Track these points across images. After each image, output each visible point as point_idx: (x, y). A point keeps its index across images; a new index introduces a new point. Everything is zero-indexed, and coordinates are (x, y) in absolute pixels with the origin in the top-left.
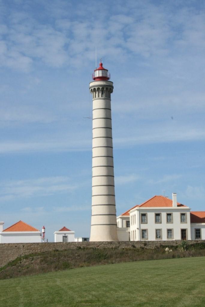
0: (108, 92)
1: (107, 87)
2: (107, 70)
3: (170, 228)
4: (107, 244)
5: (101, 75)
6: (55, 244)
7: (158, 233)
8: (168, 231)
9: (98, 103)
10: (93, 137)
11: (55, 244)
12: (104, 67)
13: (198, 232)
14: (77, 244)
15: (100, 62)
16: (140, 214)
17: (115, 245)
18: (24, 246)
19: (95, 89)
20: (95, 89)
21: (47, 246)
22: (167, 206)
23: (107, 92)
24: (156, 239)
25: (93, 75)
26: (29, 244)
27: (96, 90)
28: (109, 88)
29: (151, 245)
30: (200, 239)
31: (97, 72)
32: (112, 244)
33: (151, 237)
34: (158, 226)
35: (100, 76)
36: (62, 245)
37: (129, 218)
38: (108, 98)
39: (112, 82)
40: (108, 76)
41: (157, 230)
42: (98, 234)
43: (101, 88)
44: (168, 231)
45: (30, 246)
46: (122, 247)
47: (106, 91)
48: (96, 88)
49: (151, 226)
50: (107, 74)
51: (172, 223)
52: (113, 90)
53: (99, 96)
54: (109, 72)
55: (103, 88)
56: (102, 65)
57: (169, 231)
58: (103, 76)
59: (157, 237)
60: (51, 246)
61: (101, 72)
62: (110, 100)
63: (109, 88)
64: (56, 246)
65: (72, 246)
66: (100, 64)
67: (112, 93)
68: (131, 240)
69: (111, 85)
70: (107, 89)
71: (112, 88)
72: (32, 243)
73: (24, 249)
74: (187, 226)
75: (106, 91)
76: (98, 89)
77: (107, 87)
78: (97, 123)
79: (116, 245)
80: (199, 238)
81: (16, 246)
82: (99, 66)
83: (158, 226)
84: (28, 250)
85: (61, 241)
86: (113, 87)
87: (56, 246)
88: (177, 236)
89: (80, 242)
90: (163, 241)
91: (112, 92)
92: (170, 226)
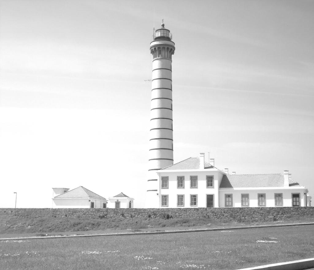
0: (169, 52)
5: (159, 35)
6: (42, 210)
7: (181, 199)
11: (42, 210)
14: (50, 210)
16: (161, 178)
17: (103, 213)
18: (12, 212)
19: (168, 48)
21: (34, 212)
22: (194, 168)
23: (168, 51)
26: (17, 210)
28: (170, 48)
29: (143, 214)
30: (184, 206)
32: (99, 212)
33: (173, 204)
34: (181, 192)
36: (48, 211)
37: (209, 186)
39: (174, 43)
41: (179, 196)
45: (18, 211)
46: (22, 211)
49: (173, 191)
50: (169, 35)
51: (197, 188)
55: (159, 48)
56: (163, 25)
57: (194, 199)
59: (178, 204)
63: (170, 48)
64: (42, 212)
65: (58, 213)
69: (173, 45)
71: (173, 49)
72: (19, 209)
73: (12, 215)
74: (215, 191)
81: (5, 212)
83: (181, 192)
84: (16, 216)
86: (174, 48)
87: (42, 212)
88: (202, 203)
89: (124, 209)
91: (173, 53)
92: (194, 192)
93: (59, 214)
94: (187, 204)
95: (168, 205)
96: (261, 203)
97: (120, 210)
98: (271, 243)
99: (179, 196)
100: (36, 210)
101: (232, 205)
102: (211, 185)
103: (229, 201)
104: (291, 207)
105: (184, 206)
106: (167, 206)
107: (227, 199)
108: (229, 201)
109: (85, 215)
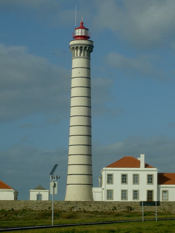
1: (90, 47)
2: (88, 29)
3: (136, 189)
4: (64, 203)
5: (83, 34)
7: (124, 193)
8: (149, 193)
9: (78, 62)
10: (72, 97)
12: (85, 26)
13: (150, 193)
15: (81, 21)
17: (72, 205)
19: (73, 48)
20: (73, 48)
24: (107, 200)
25: (74, 33)
27: (75, 48)
30: (113, 200)
31: (80, 30)
32: (69, 204)
33: (117, 198)
35: (82, 35)
38: (89, 58)
40: (89, 36)
41: (122, 191)
42: (74, 193)
43: (84, 47)
44: (149, 193)
47: (89, 49)
48: (75, 47)
52: (94, 49)
53: (80, 55)
54: (89, 31)
55: (86, 48)
56: (82, 24)
57: (136, 193)
58: (86, 35)
59: (122, 198)
60: (9, 204)
61: (83, 30)
62: (90, 59)
66: (81, 23)
67: (92, 51)
68: (155, 199)
70: (89, 48)
74: (154, 187)
75: (89, 49)
76: (81, 47)
77: (90, 47)
78: (77, 82)
79: (73, 204)
80: (136, 199)
82: (80, 25)
85: (48, 200)
89: (33, 201)
90: (129, 202)
92: (124, 187)
93: (31, 206)
94: (130, 198)
95: (113, 199)
96: (164, 197)
97: (88, 203)
98: (30, 220)
99: (122, 191)
100: (7, 202)
101: (168, 199)
102: (125, 182)
103: (165, 196)
104: (12, 201)
105: (113, 200)
106: (112, 200)
107: (164, 194)
108: (165, 196)
109: (56, 207)
